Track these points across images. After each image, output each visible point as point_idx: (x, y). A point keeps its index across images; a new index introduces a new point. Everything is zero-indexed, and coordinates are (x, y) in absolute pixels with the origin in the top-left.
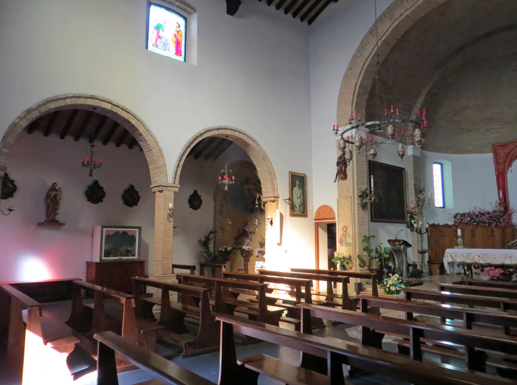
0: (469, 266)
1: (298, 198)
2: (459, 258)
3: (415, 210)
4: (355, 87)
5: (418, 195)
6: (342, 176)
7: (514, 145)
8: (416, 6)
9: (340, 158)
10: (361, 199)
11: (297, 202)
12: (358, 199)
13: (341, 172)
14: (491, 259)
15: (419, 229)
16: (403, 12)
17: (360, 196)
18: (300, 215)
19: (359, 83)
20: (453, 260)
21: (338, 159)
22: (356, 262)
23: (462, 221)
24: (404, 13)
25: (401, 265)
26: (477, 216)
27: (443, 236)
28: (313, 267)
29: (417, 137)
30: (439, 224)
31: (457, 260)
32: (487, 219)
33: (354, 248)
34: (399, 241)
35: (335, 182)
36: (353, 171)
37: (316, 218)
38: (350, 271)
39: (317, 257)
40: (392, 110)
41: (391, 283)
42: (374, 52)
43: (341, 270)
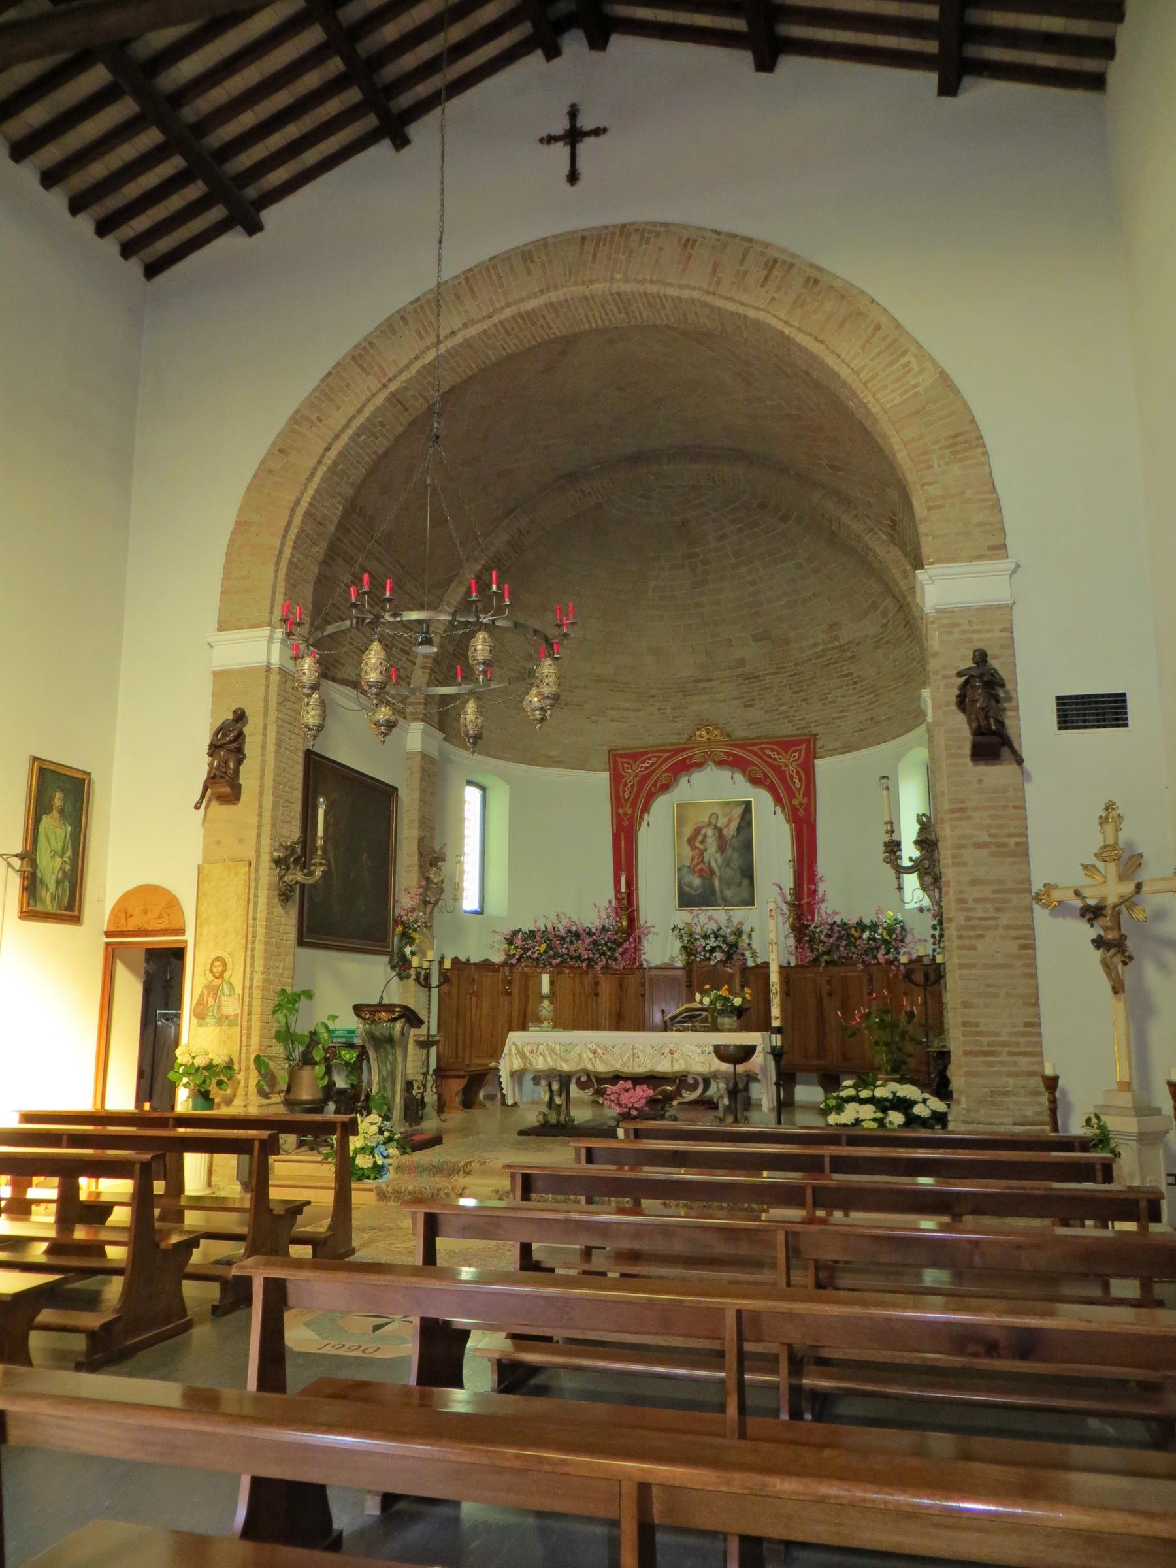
0: (565, 1080)
1: (54, 853)
2: (541, 1058)
3: (415, 915)
4: (293, 511)
5: (428, 872)
6: (226, 790)
7: (659, 757)
8: (496, 319)
9: (223, 729)
10: (280, 872)
11: (50, 866)
12: (272, 869)
13: (221, 777)
14: (625, 1059)
15: (423, 973)
16: (457, 323)
17: (277, 862)
18: (56, 914)
19: (304, 503)
20: (525, 1065)
21: (216, 734)
22: (247, 1079)
23: (524, 953)
24: (460, 330)
25: (388, 1084)
26: (563, 939)
27: (475, 994)
28: (84, 1103)
29: (548, 684)
30: (468, 960)
31: (537, 1062)
32: (587, 949)
33: (244, 1032)
34: (389, 1008)
35: (197, 807)
36: (262, 777)
37: (113, 929)
38: (224, 1111)
39: (101, 1066)
40: (494, 587)
41: (359, 1145)
42: (361, 420)
43: (195, 1108)
